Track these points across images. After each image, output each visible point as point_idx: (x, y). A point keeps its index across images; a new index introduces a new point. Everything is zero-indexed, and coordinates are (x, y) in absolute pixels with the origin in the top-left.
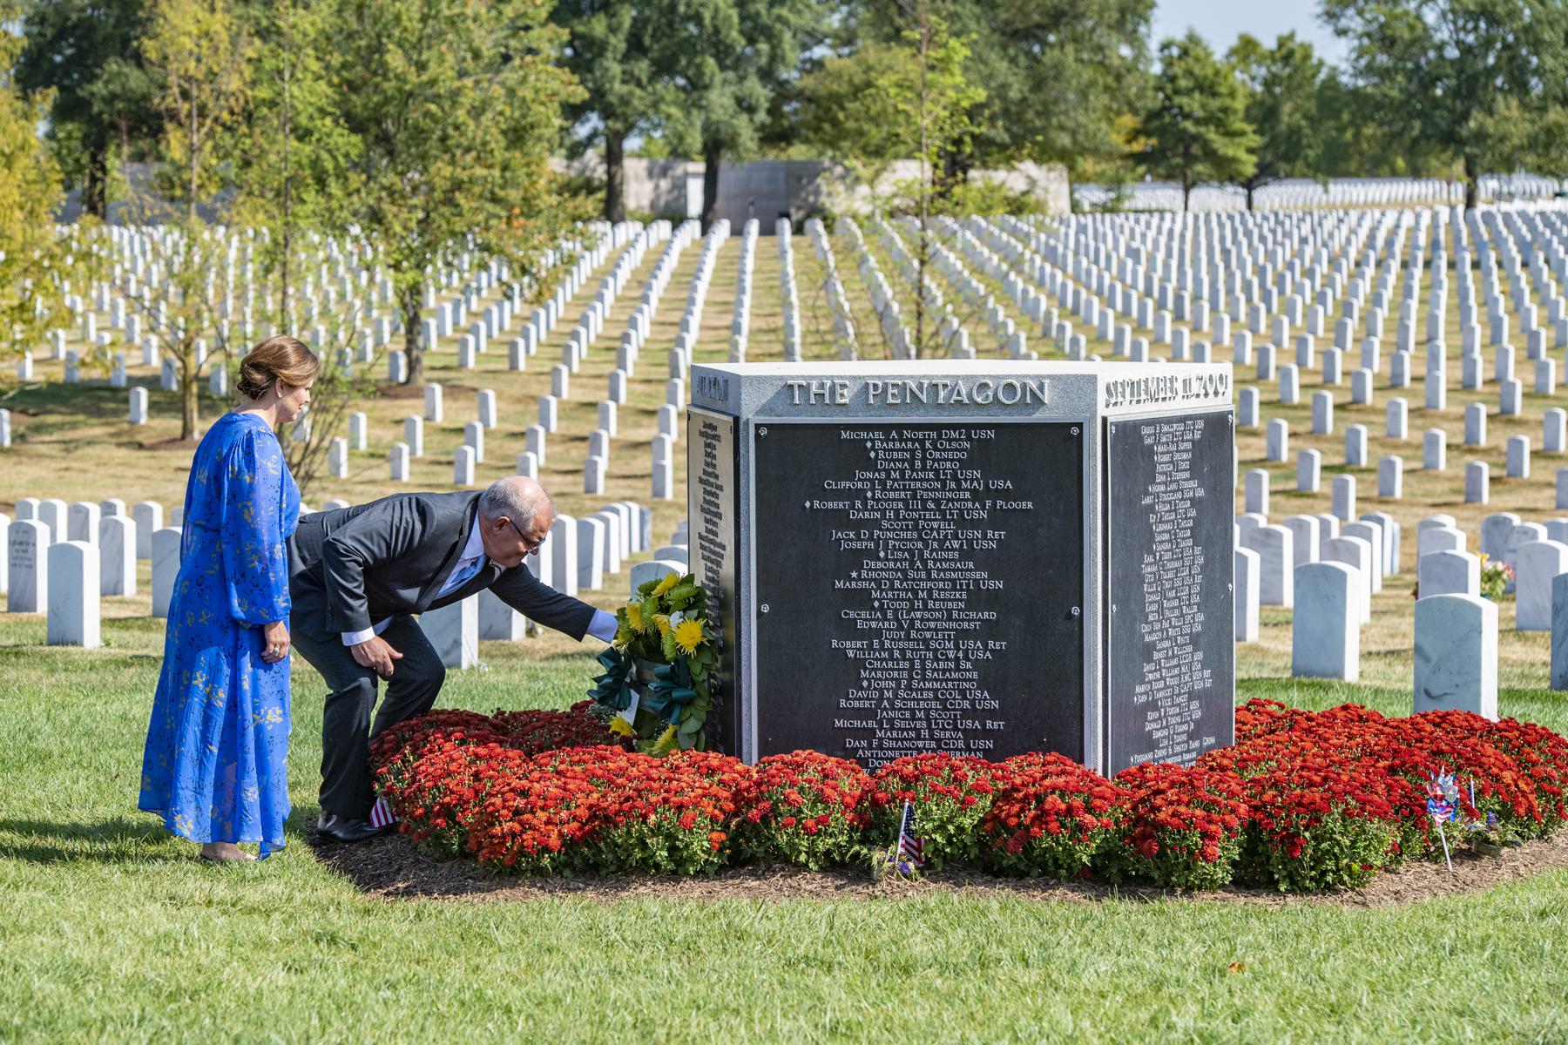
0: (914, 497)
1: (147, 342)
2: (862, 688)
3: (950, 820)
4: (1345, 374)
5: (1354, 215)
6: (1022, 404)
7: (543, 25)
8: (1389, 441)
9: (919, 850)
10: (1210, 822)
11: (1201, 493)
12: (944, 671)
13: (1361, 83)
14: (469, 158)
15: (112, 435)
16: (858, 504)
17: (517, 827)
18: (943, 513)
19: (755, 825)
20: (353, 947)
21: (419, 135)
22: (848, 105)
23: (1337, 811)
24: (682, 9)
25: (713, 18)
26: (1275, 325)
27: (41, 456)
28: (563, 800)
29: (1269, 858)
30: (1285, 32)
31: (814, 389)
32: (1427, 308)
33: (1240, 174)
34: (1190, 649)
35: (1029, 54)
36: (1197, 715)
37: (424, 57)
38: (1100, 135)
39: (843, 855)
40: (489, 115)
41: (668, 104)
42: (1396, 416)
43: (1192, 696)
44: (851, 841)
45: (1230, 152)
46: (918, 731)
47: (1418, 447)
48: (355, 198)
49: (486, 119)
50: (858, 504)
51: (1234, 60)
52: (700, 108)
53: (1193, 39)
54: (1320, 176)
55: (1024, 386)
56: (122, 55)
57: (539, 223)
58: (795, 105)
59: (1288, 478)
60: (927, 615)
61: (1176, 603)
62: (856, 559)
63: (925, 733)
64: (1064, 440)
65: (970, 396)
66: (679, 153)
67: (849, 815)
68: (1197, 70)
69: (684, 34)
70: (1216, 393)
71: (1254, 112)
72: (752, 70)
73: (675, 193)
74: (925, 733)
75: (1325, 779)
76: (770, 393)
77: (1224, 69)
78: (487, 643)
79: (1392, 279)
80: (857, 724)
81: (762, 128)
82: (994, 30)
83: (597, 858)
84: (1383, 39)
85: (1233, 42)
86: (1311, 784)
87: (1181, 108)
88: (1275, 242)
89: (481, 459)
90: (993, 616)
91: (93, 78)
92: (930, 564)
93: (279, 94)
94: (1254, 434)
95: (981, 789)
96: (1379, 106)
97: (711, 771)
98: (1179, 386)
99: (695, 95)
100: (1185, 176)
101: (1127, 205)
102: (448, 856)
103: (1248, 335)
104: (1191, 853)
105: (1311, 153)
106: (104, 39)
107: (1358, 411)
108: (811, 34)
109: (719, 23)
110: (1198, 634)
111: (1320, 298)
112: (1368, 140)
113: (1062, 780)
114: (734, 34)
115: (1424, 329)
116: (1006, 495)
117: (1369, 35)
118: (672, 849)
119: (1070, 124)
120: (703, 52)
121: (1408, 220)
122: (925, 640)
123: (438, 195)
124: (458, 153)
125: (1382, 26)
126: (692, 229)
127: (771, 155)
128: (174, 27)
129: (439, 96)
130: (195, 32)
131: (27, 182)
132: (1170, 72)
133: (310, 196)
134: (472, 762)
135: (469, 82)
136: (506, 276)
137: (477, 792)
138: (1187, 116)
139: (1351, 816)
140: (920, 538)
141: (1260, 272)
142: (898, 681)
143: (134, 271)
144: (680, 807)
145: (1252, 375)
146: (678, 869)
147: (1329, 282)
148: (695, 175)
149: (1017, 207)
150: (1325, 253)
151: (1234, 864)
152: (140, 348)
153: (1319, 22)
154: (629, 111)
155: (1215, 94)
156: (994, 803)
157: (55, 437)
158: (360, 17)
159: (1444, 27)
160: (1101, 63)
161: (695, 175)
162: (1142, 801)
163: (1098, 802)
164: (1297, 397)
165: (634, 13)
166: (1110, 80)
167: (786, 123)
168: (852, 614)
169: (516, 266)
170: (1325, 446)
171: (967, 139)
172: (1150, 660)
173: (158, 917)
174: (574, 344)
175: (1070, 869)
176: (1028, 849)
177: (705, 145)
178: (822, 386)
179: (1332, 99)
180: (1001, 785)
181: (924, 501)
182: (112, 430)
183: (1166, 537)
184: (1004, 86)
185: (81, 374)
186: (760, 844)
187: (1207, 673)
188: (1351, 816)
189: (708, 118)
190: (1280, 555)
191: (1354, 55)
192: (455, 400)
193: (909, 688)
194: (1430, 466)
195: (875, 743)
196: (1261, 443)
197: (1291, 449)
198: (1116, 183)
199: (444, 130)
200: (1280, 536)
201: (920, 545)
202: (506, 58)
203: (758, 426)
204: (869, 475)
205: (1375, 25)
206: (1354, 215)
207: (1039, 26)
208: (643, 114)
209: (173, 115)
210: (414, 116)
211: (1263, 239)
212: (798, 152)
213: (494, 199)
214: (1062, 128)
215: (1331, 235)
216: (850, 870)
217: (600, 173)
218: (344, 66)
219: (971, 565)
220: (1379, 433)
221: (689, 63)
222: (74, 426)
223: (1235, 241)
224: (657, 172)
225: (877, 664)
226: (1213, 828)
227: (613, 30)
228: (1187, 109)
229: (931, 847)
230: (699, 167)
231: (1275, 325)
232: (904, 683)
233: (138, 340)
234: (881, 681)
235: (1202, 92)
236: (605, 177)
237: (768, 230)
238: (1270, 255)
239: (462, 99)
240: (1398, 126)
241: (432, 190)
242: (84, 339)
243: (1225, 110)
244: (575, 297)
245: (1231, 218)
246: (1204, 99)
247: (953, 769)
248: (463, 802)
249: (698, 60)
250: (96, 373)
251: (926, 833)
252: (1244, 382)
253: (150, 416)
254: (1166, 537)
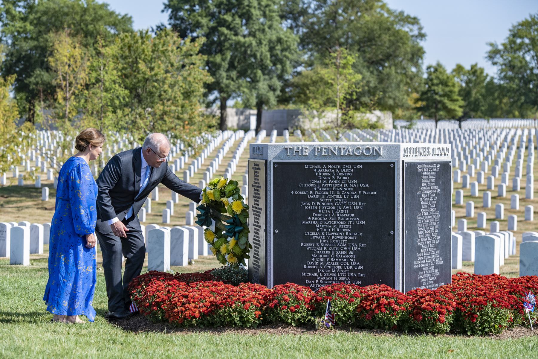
0: (332, 190)
1: (49, 171)
2: (312, 261)
3: (345, 307)
4: (495, 186)
5: (499, 131)
6: (372, 156)
7: (197, 54)
8: (512, 210)
9: (333, 319)
10: (442, 308)
11: (439, 191)
12: (343, 255)
13: (502, 82)
14: (169, 103)
15: (35, 205)
16: (311, 192)
17: (183, 309)
18: (343, 196)
19: (272, 309)
20: (122, 344)
21: (151, 94)
22: (311, 88)
23: (489, 305)
24: (249, 52)
25: (261, 56)
26: (469, 168)
27: (9, 212)
28: (201, 299)
29: (464, 322)
30: (474, 63)
31: (295, 149)
32: (526, 163)
33: (456, 115)
34: (435, 249)
35: (377, 70)
36: (437, 274)
37: (153, 65)
38: (404, 101)
39: (304, 320)
40: (177, 87)
41: (243, 87)
42: (515, 201)
43: (435, 267)
44: (307, 315)
45: (453, 107)
46: (333, 277)
47: (523, 212)
48: (127, 117)
49: (176, 88)
50: (311, 192)
51: (454, 73)
52: (255, 89)
53: (439, 65)
54: (486, 117)
55: (373, 149)
56: (41, 68)
57: (195, 128)
58: (291, 88)
59: (474, 223)
60: (336, 234)
61: (429, 232)
62: (310, 213)
63: (336, 278)
64: (386, 170)
65: (353, 152)
66: (247, 106)
67: (307, 306)
68: (441, 77)
69: (250, 62)
70: (445, 155)
71: (462, 93)
72: (275, 75)
73: (246, 121)
74: (336, 278)
75: (485, 293)
76: (279, 151)
77: (451, 76)
78: (174, 267)
79: (513, 152)
80: (310, 274)
81: (278, 97)
82: (365, 61)
83: (213, 320)
84: (510, 66)
85: (454, 67)
86: (480, 295)
87: (434, 90)
88: (469, 139)
89: (172, 214)
90: (361, 234)
91: (30, 76)
92: (338, 215)
93: (99, 75)
94: (461, 207)
95: (356, 296)
96: (509, 91)
97: (256, 290)
98: (431, 151)
99: (253, 84)
100: (436, 117)
101: (414, 127)
102: (158, 321)
103: (459, 171)
104: (434, 320)
105: (483, 108)
106: (35, 62)
107: (500, 199)
108: (296, 62)
109: (263, 57)
110: (438, 244)
111: (486, 158)
112: (505, 104)
113: (386, 293)
114: (268, 62)
115: (525, 170)
116: (366, 189)
117: (505, 65)
118: (241, 317)
119: (393, 96)
120: (257, 68)
121: (519, 132)
122: (336, 243)
123: (157, 116)
124: (165, 101)
125: (510, 62)
126: (251, 134)
127: (282, 107)
128: (61, 54)
129: (158, 80)
130: (68, 55)
131: (5, 111)
132: (430, 77)
133: (110, 114)
134: (167, 287)
135: (169, 75)
136: (182, 148)
137: (169, 297)
138: (437, 94)
139: (495, 307)
140: (334, 205)
141: (464, 149)
142: (326, 258)
143: (44, 146)
144: (244, 302)
145: (461, 186)
146: (243, 325)
147: (490, 153)
148: (253, 115)
149: (373, 127)
150: (488, 143)
151: (451, 324)
152: (46, 174)
153: (486, 60)
154: (229, 90)
155: (447, 86)
156: (361, 301)
157: (14, 205)
158: (130, 50)
159: (533, 62)
160: (405, 74)
161: (253, 115)
162: (416, 300)
163: (400, 301)
164: (477, 194)
165: (231, 54)
166: (408, 80)
167: (287, 95)
168: (309, 234)
169: (186, 143)
170: (488, 212)
171: (354, 93)
172: (420, 252)
173: (49, 336)
174: (208, 173)
175: (389, 326)
176: (374, 318)
177: (257, 103)
178: (298, 148)
179: (491, 88)
180: (363, 295)
181: (336, 191)
182: (35, 203)
183: (426, 207)
184: (368, 82)
185: (24, 183)
186: (274, 316)
187: (441, 259)
188: (495, 307)
189: (258, 93)
190: (470, 242)
191: (499, 72)
192: (163, 193)
193: (330, 261)
194: (527, 219)
195: (317, 281)
196: (464, 210)
197: (475, 213)
198: (410, 119)
199: (160, 92)
200: (470, 235)
201: (334, 208)
202: (183, 66)
203: (274, 163)
204: (315, 182)
205: (507, 61)
206: (499, 131)
207: (382, 60)
208: (234, 91)
209: (60, 86)
210: (149, 88)
211: (465, 138)
212: (291, 106)
213: (178, 118)
214: (390, 97)
215: (490, 137)
216: (308, 326)
217: (218, 113)
218: (123, 68)
219: (353, 215)
220: (508, 207)
221: (252, 72)
222: (21, 201)
223: (454, 139)
224: (239, 113)
225: (318, 252)
226: (443, 310)
227: (223, 60)
228: (436, 91)
229: (337, 317)
230: (255, 111)
231: (469, 168)
232: (328, 259)
233: (45, 170)
234: (319, 259)
235: (442, 85)
237: (280, 134)
238: (468, 144)
239: (167, 81)
240: (516, 98)
241: (156, 114)
242: (26, 169)
243: (451, 92)
244: (208, 157)
245: (453, 131)
246: (443, 87)
247: (346, 288)
248: (163, 301)
249: (255, 71)
250: (29, 182)
251: (335, 312)
252: (457, 188)
253: (49, 198)
254: (426, 207)
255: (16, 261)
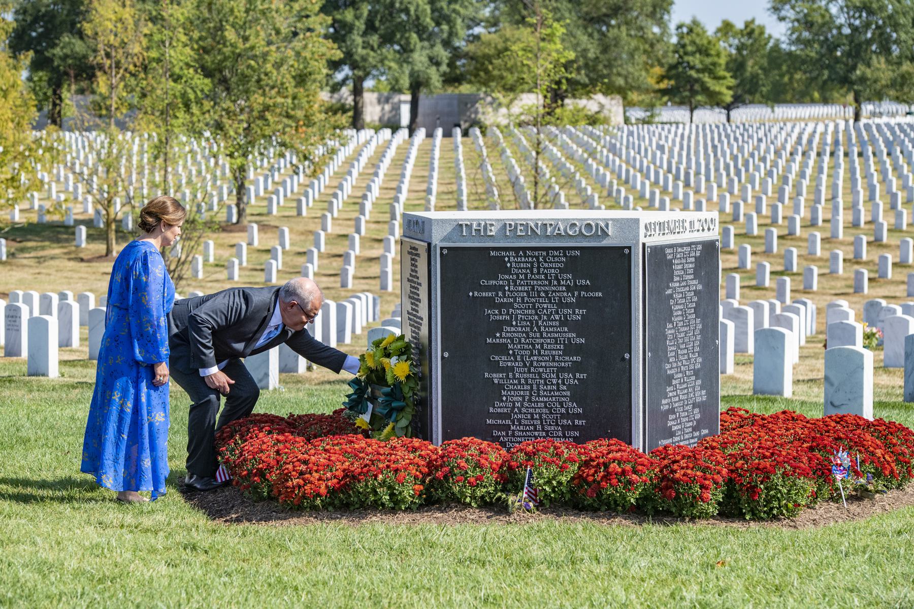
0: (533, 290)
1: (86, 199)
2: (502, 401)
3: (554, 478)
4: (784, 218)
5: (789, 125)
6: (596, 236)
7: (316, 15)
8: (810, 257)
9: (536, 495)
10: (705, 479)
11: (700, 287)
12: (550, 391)
13: (793, 48)
14: (274, 92)
15: (65, 254)
16: (500, 294)
17: (301, 482)
18: (550, 299)
19: (440, 481)
20: (206, 552)
21: (244, 79)
22: (495, 61)
23: (779, 473)
24: (397, 5)
25: (416, 11)
26: (743, 189)
27: (24, 266)
28: (328, 466)
29: (740, 500)
30: (749, 19)
31: (474, 227)
32: (832, 179)
33: (723, 101)
34: (693, 378)
35: (600, 31)
36: (698, 417)
37: (247, 33)
38: (641, 79)
39: (491, 498)
40: (285, 67)
41: (389, 61)
42: (814, 242)
43: (695, 405)
44: (496, 490)
45: (717, 89)
46: (535, 426)
47: (827, 260)
48: (207, 116)
49: (283, 69)
50: (500, 294)
51: (719, 35)
52: (408, 63)
53: (695, 22)
54: (769, 102)
55: (597, 225)
56: (71, 32)
57: (314, 130)
58: (463, 61)
59: (751, 278)
60: (540, 358)
61: (685, 351)
62: (499, 326)
63: (539, 427)
64: (620, 257)
65: (565, 231)
66: (396, 89)
67: (495, 475)
68: (698, 41)
69: (399, 20)
70: (709, 229)
71: (731, 65)
72: (438, 41)
73: (394, 113)
74: (539, 427)
75: (772, 454)
76: (449, 229)
77: (714, 40)
79: (811, 163)
80: (499, 422)
81: (444, 74)
82: (579, 18)
83: (348, 500)
84: (806, 23)
85: (719, 24)
86: (764, 457)
87: (688, 63)
88: (743, 141)
89: (280, 267)
90: (579, 359)
91: (54, 45)
92: (542, 329)
93: (163, 55)
94: (731, 253)
95: (572, 460)
96: (804, 62)
97: (415, 449)
98: (687, 225)
99: (405, 55)
100: (691, 102)
102: (261, 499)
103: (728, 195)
104: (694, 497)
105: (764, 89)
106: (61, 23)
107: (792, 239)
108: (472, 20)
109: (419, 13)
110: (698, 370)
111: (769, 174)
112: (798, 82)
113: (619, 454)
114: (428, 20)
115: (830, 192)
116: (586, 288)
117: (798, 20)
118: (392, 495)
119: (624, 72)
120: (410, 30)
121: (821, 128)
122: (539, 373)
123: (255, 114)
124: (267, 89)
125: (806, 15)
126: (403, 133)
127: (450, 90)
128: (102, 16)
129: (256, 56)
130: (114, 18)
132: (682, 42)
133: (181, 114)
134: (275, 444)
135: (273, 48)
136: (295, 161)
137: (278, 462)
138: (692, 68)
139: (788, 475)
140: (537, 314)
141: (735, 158)
142: (524, 397)
143: (78, 158)
144: (396, 471)
145: (730, 218)
146: (395, 506)
147: (775, 164)
148: (405, 102)
149: (593, 120)
150: (772, 147)
151: (719, 503)
152: (81, 203)
153: (769, 13)
154: (367, 65)
155: (708, 55)
156: (579, 468)
157: (32, 255)
158: (210, 10)
159: (842, 16)
160: (642, 37)
161: (405, 102)
162: (666, 467)
163: (640, 468)
164: (756, 232)
165: (370, 7)
166: (647, 47)
167: (458, 72)
168: (497, 358)
169: (301, 155)
170: (772, 260)
171: (564, 81)
172: (670, 385)
173: (92, 534)
174: (335, 201)
175: (623, 506)
176: (600, 495)
177: (411, 85)
178: (479, 225)
179: (776, 57)
180: (583, 458)
181: (539, 292)
182: (65, 250)
183: (680, 313)
184: (585, 50)
185: (47, 218)
186: (443, 492)
187: (704, 392)
188: (788, 475)
189: (413, 69)
190: (746, 324)
191: (789, 32)
192: (265, 233)
193: (530, 401)
194: (834, 272)
195: (510, 433)
196: (735, 258)
197: (752, 262)
198: (651, 107)
199: (259, 76)
200: (746, 313)
201: (536, 318)
202: (295, 34)
203: (442, 249)
204: (507, 277)
205: (802, 15)
206: (789, 125)
207: (606, 15)
208: (375, 67)
209: (101, 67)
210: (241, 67)
211: (736, 139)
212: (465, 89)
213: (288, 116)
214: (619, 74)
215: (776, 137)
216: (495, 507)
217: (350, 101)
218: (201, 38)
219: (566, 329)
220: (804, 252)
221: (402, 37)
222: (43, 248)
223: (720, 140)
224: (383, 100)
225: (511, 387)
226: (707, 482)
227: (357, 17)
228: (692, 64)
229: (543, 494)
230: (407, 97)
231: (743, 189)
232: (527, 398)
233: (80, 198)
234: (513, 397)
235: (700, 54)
236: (352, 103)
237: (447, 134)
238: (741, 149)
239: (269, 58)
240: (815, 74)
241: (252, 110)
242: (49, 198)
243: (714, 64)
244: (335, 173)
245: (717, 127)
246: (702, 58)
247: (556, 448)
248: (270, 467)
249: (407, 35)
250: (56, 218)
251: (540, 485)
252: (725, 222)
253: (88, 242)
254: (680, 313)
255: (37, 369)
